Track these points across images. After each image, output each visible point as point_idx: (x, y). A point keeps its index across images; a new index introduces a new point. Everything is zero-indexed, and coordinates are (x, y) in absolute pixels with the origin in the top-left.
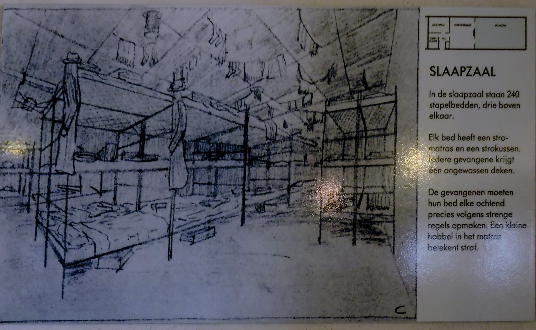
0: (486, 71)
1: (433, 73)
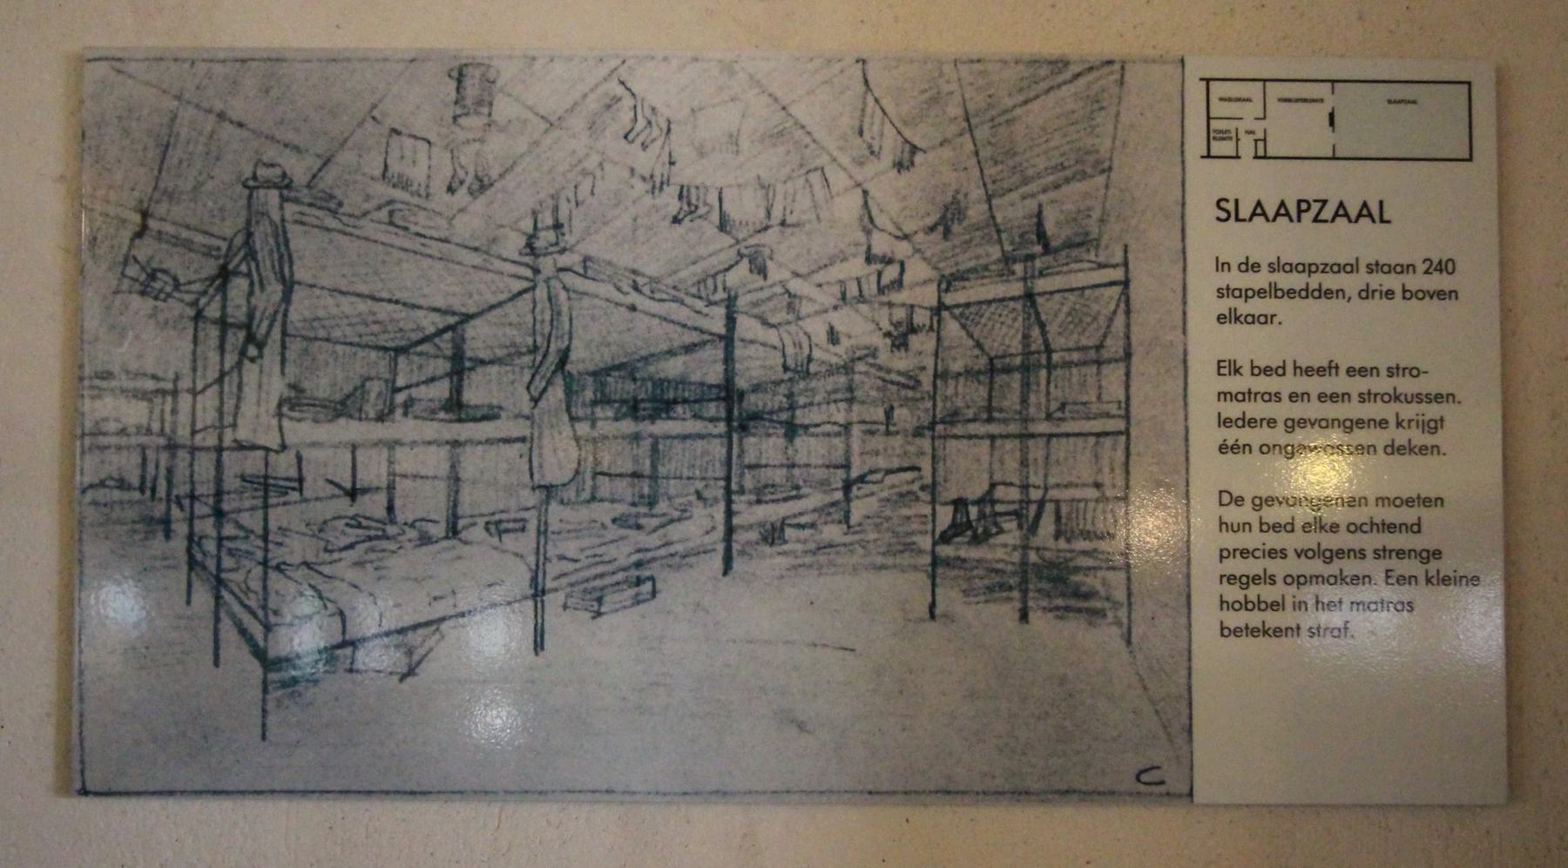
0: (1365, 211)
1: (1224, 215)
